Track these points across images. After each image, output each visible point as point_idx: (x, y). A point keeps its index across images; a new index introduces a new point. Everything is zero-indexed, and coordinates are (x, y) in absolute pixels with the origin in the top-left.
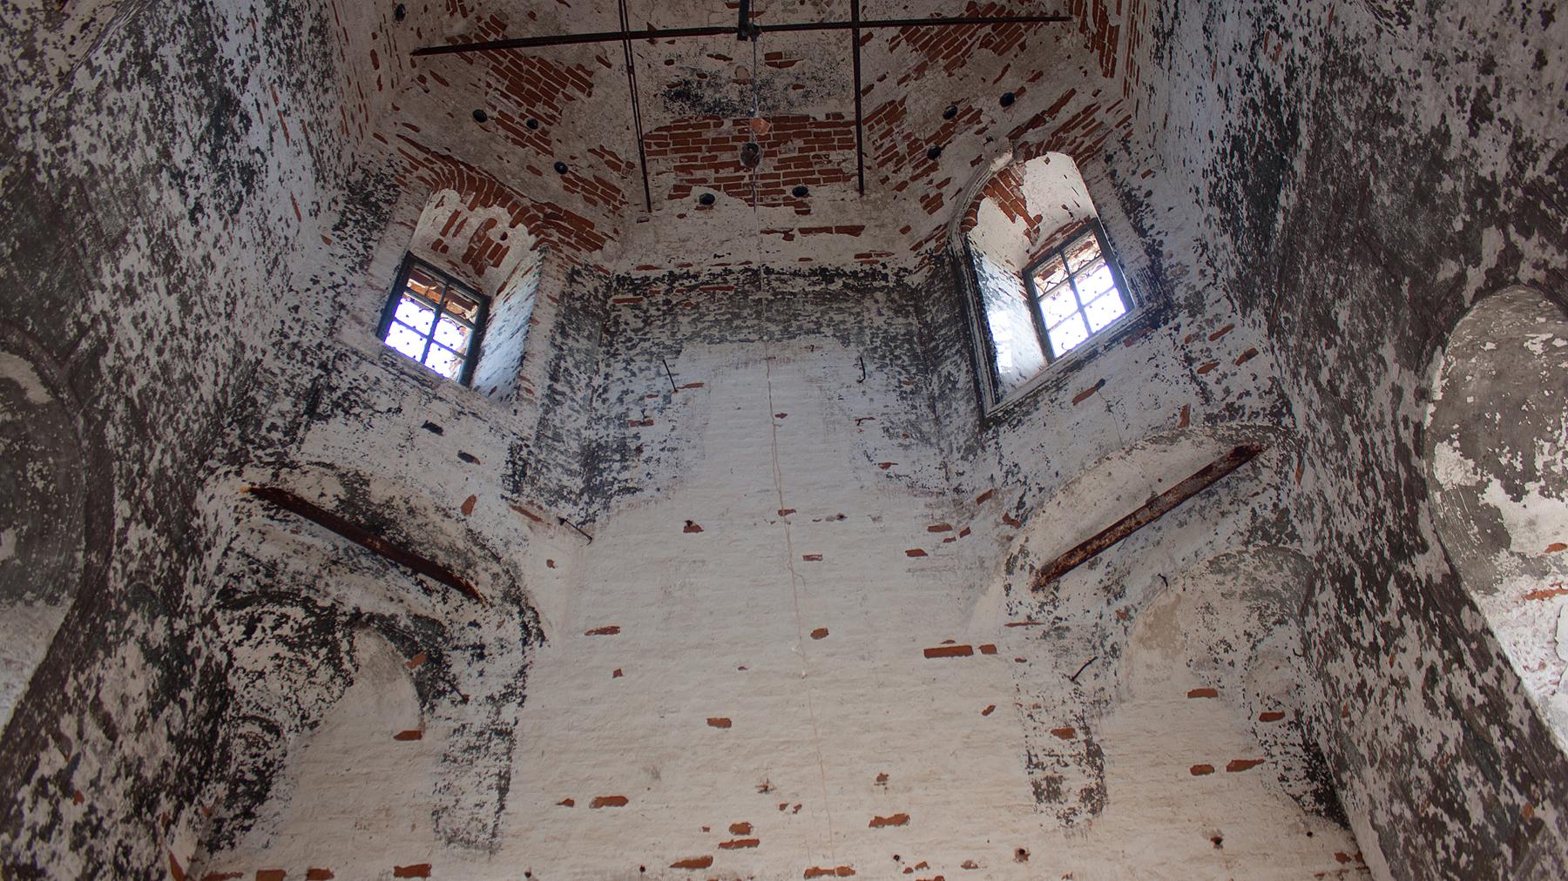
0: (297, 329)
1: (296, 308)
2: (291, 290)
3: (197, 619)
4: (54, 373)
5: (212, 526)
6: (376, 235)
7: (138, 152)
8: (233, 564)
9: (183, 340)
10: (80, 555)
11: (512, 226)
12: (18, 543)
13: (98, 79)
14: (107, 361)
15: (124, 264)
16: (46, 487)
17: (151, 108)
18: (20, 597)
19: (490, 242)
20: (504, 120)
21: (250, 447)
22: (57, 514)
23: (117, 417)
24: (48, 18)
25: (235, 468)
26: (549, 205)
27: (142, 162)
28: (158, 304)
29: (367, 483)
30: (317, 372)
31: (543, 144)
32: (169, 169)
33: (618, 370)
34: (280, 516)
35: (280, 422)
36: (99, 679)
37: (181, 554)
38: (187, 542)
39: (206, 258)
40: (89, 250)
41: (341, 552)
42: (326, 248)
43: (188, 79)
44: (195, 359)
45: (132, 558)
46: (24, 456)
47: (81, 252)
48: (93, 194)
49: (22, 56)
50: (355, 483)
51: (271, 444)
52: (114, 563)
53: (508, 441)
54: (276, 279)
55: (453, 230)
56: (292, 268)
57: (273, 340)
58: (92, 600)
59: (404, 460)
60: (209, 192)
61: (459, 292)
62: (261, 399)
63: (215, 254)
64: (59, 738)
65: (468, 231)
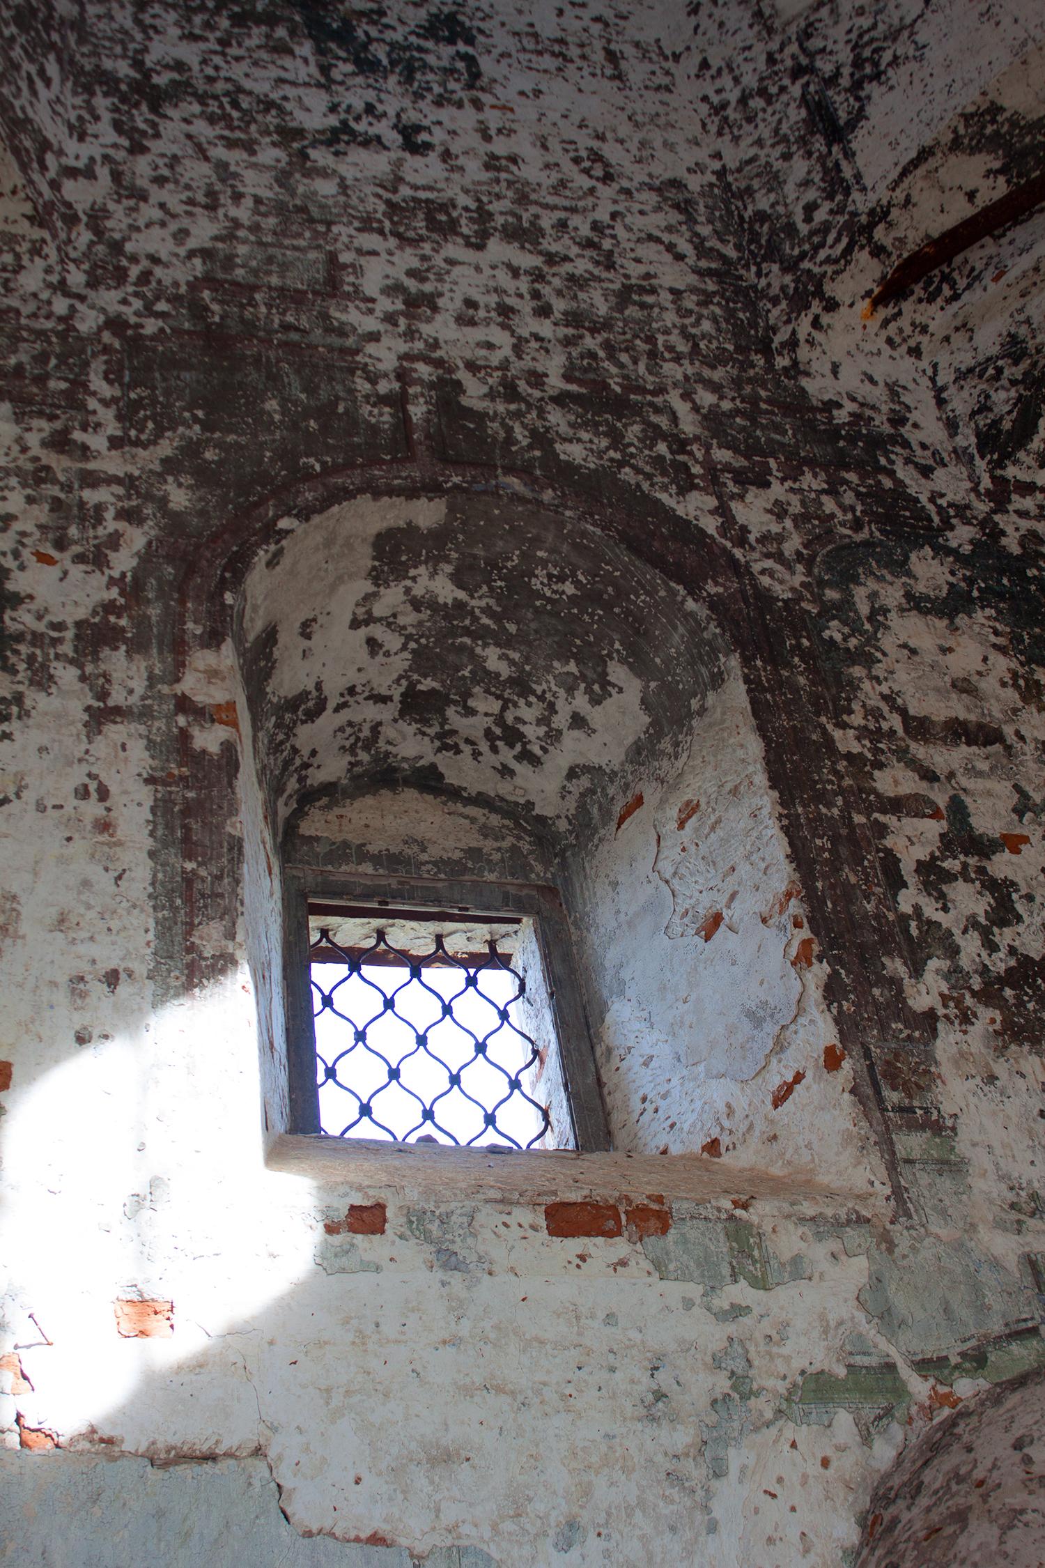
0: (726, 81)
1: (705, 65)
2: (676, 57)
3: (982, 507)
4: (413, 472)
5: (877, 395)
7: (249, 176)
8: (961, 402)
9: (567, 268)
10: (690, 605)
13: (103, 172)
14: (474, 393)
15: (371, 286)
16: (577, 583)
17: (212, 120)
18: (690, 715)
21: (806, 265)
22: (622, 594)
23: (564, 429)
25: (816, 307)
27: (267, 178)
28: (472, 273)
29: (995, 109)
30: (796, 90)
32: (314, 144)
34: (962, 283)
35: (811, 195)
36: (888, 699)
37: (859, 467)
38: (854, 447)
39: (492, 163)
40: (304, 323)
43: (224, 43)
44: (610, 266)
45: (780, 538)
46: (518, 581)
47: (294, 336)
48: (240, 272)
50: (982, 128)
51: (825, 228)
52: (756, 568)
54: (637, 71)
56: (647, 37)
57: (713, 129)
58: (760, 630)
59: (1007, 22)
60: (407, 103)
62: (763, 202)
63: (500, 147)
64: (896, 805)
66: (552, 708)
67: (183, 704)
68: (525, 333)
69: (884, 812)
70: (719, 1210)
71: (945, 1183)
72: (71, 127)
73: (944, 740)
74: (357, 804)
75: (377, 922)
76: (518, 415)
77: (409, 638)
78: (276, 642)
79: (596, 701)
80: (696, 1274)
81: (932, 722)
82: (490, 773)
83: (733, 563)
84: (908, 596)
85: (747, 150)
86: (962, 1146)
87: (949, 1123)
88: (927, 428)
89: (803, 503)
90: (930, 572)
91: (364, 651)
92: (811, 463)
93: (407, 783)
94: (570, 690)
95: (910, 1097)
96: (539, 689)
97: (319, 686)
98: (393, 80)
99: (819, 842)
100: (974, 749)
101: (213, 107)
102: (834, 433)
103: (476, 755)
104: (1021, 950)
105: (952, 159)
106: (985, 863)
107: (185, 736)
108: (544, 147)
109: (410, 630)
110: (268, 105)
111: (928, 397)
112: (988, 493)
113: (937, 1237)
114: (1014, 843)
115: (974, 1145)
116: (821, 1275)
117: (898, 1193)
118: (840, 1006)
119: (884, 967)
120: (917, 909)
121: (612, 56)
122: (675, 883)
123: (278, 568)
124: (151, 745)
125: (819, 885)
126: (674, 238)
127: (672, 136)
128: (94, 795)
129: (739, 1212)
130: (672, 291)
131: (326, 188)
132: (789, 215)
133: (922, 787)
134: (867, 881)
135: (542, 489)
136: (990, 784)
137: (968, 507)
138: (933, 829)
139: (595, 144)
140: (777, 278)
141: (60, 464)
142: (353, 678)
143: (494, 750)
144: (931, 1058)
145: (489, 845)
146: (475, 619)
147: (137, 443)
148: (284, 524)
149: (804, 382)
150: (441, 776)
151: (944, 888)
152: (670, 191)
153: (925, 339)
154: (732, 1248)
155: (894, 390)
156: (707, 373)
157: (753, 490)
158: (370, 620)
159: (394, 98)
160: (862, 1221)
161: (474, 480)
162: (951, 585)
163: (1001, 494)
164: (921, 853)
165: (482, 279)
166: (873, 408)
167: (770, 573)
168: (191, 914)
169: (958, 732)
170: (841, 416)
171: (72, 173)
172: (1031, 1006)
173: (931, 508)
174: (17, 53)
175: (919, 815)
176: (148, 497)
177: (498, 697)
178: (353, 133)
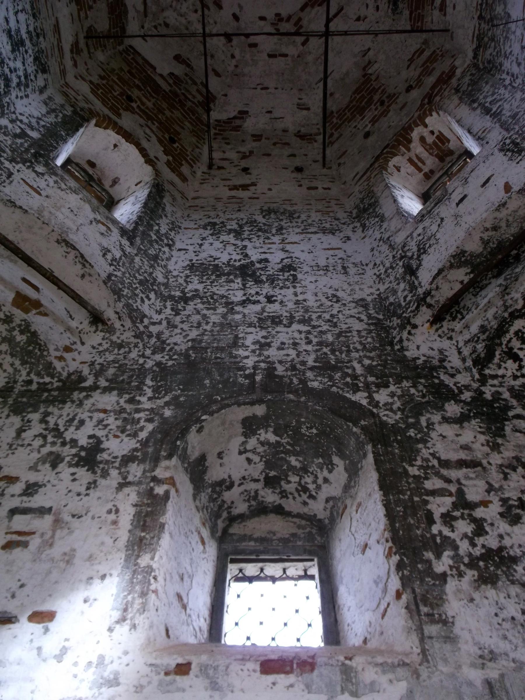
0: (381, 267)
2: (367, 265)
6: (377, 210)
8: (466, 352)
9: (320, 329)
10: (355, 429)
11: (426, 126)
12: (340, 456)
14: (280, 370)
15: (248, 342)
16: (317, 429)
17: (203, 303)
18: (358, 471)
19: (434, 143)
20: (374, 121)
21: (404, 315)
24: (110, 332)
25: (409, 328)
26: (423, 100)
27: (219, 316)
28: (283, 335)
29: (463, 252)
30: (401, 264)
31: (393, 97)
32: (236, 306)
33: (507, 65)
35: (406, 293)
36: (433, 455)
37: (425, 377)
38: (425, 372)
39: (297, 302)
40: (223, 356)
41: (504, 283)
42: (366, 239)
45: (392, 404)
46: (297, 431)
47: (219, 360)
48: (203, 344)
49: (119, 350)
50: (459, 259)
51: (410, 301)
52: (381, 414)
53: (496, 151)
54: (352, 270)
55: (420, 164)
56: (357, 261)
58: (381, 435)
60: (270, 290)
61: (455, 169)
62: (392, 300)
63: (300, 297)
64: (433, 493)
65: (424, 155)
66: (316, 477)
67: (154, 479)
68: (301, 350)
69: (427, 495)
70: (338, 661)
71: (448, 647)
72: (157, 311)
73: (456, 468)
74: (252, 521)
75: (260, 565)
76: (295, 375)
77: (262, 457)
78: (206, 460)
79: (330, 471)
80: (325, 690)
81: (451, 461)
82: (300, 505)
83: (373, 414)
84: (443, 418)
85: (387, 286)
86: (457, 630)
87: (451, 620)
88: (455, 361)
89: (402, 391)
90: (453, 409)
91: (246, 463)
92: (407, 378)
93: (272, 511)
94: (321, 469)
95: (433, 609)
96: (311, 470)
97: (230, 477)
98: (267, 284)
99: (398, 509)
100: (469, 470)
101: (205, 300)
102: (417, 367)
103: (294, 498)
104: (488, 546)
105: (452, 272)
106: (472, 512)
107: (152, 489)
108: (316, 295)
109: (262, 454)
110: (223, 297)
111: (455, 352)
112: (478, 380)
113: (442, 672)
114: (485, 504)
115: (462, 629)
116: (384, 690)
117: (424, 652)
118: (403, 573)
119: (423, 555)
120: (440, 532)
121: (344, 268)
122: (356, 535)
123: (203, 433)
124: (139, 493)
125: (397, 525)
126: (360, 315)
127: (362, 286)
128: (113, 512)
129: (347, 662)
130: (357, 331)
131: (238, 317)
132: (399, 301)
133: (445, 485)
134: (418, 522)
135: (301, 397)
136: (475, 482)
137: (470, 386)
138: (448, 501)
139: (334, 292)
140: (396, 321)
141: (129, 407)
142: (243, 473)
143: (300, 495)
144: (444, 592)
145: (300, 532)
146: (284, 447)
147: (158, 398)
148: (204, 417)
149: (406, 353)
150: (283, 508)
151: (453, 523)
152: (362, 303)
153: (453, 334)
154: (342, 679)
155: (441, 351)
156: (368, 354)
157: (382, 389)
158: (246, 451)
159: (266, 289)
160: (405, 664)
161: (276, 397)
162: (461, 413)
163: (483, 380)
164: (443, 510)
165: (288, 336)
166: (433, 358)
167: (387, 415)
168: (139, 552)
169: (461, 464)
170: (419, 362)
171: (154, 324)
172: (492, 569)
173: (454, 388)
174: (138, 291)
175: (443, 495)
176: (157, 414)
177: (298, 475)
178: (250, 300)
